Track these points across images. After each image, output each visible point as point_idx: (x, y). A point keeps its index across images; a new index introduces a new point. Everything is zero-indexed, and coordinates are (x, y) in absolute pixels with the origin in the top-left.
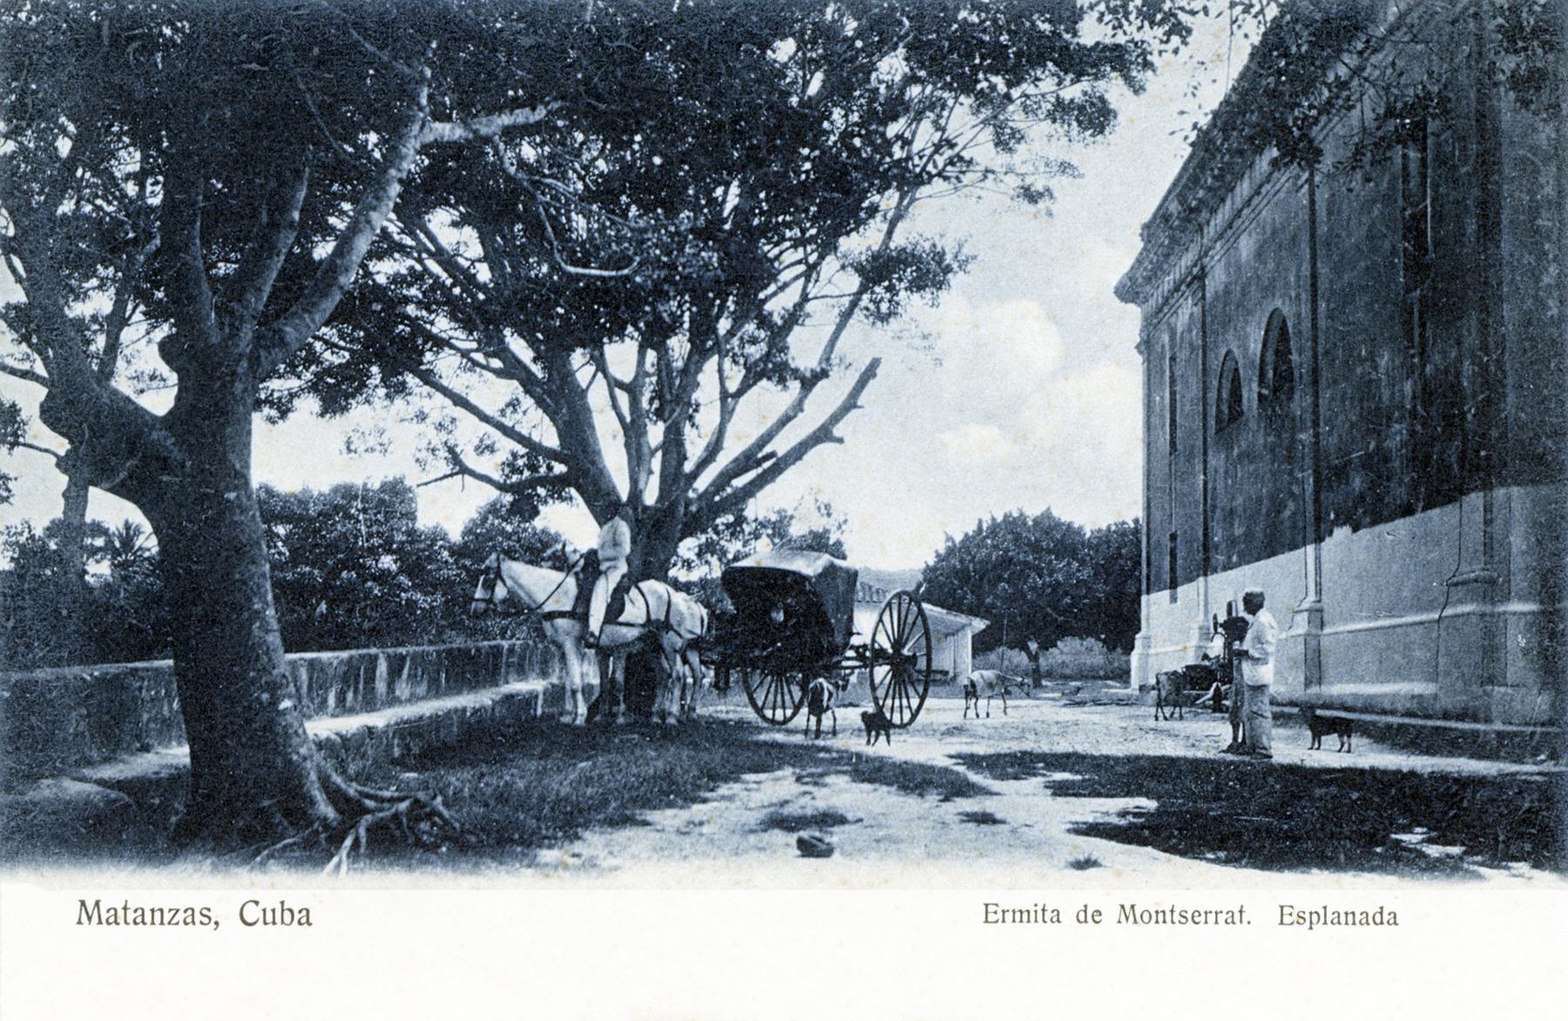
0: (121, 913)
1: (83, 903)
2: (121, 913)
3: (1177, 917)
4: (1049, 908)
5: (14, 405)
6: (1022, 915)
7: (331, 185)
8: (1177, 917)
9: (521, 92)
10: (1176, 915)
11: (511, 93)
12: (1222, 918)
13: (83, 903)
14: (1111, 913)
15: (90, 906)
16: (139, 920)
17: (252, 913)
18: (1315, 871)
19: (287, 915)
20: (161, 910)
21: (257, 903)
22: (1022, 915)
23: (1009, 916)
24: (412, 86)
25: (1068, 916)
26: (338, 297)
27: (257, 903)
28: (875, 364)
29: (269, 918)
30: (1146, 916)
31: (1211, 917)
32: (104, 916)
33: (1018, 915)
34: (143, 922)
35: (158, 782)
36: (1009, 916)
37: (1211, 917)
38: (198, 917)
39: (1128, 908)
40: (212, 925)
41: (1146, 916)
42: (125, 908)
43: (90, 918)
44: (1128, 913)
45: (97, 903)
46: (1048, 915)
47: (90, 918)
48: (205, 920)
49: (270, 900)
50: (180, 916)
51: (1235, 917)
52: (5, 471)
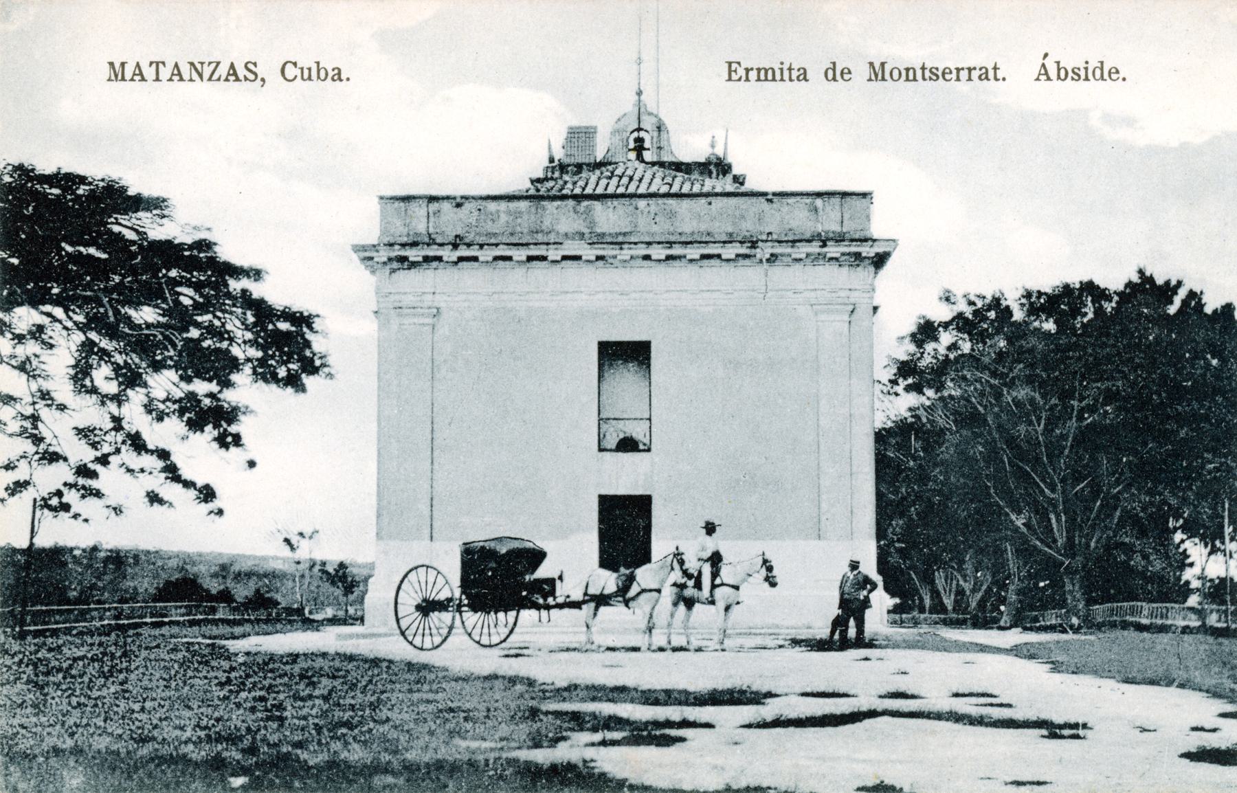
3: (927, 74)
5: (137, 432)
7: (24, 232)
12: (975, 74)
14: (861, 72)
18: (1223, 748)
20: (924, 79)
21: (295, 64)
23: (753, 75)
25: (815, 74)
27: (295, 64)
28: (1195, 729)
30: (896, 73)
31: (964, 74)
36: (753, 75)
37: (964, 74)
40: (258, 81)
41: (896, 73)
45: (883, 64)
46: (795, 74)
48: (252, 77)
52: (6, 390)
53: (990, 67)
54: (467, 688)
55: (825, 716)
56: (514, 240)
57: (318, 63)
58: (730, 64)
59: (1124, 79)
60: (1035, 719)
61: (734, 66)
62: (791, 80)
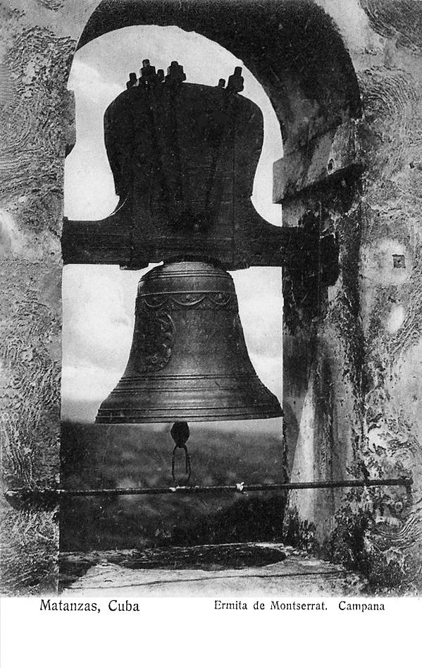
0: (58, 605)
1: (43, 601)
2: (58, 605)
3: (296, 607)
4: (242, 603)
6: (229, 606)
8: (296, 607)
9: (145, 530)
10: (296, 606)
11: (141, 527)
13: (43, 601)
14: (268, 605)
15: (46, 602)
16: (136, 609)
17: (114, 606)
19: (129, 606)
21: (116, 601)
22: (229, 606)
24: (217, 482)
25: (250, 606)
26: (234, 487)
27: (116, 601)
29: (121, 608)
31: (310, 607)
32: (51, 607)
33: (229, 606)
34: (72, 604)
35: (217, 562)
36: (225, 606)
38: (91, 607)
39: (275, 603)
41: (283, 607)
42: (60, 603)
43: (45, 608)
44: (275, 605)
46: (242, 606)
47: (45, 608)
48: (94, 609)
49: (122, 601)
50: (83, 607)
51: (321, 607)
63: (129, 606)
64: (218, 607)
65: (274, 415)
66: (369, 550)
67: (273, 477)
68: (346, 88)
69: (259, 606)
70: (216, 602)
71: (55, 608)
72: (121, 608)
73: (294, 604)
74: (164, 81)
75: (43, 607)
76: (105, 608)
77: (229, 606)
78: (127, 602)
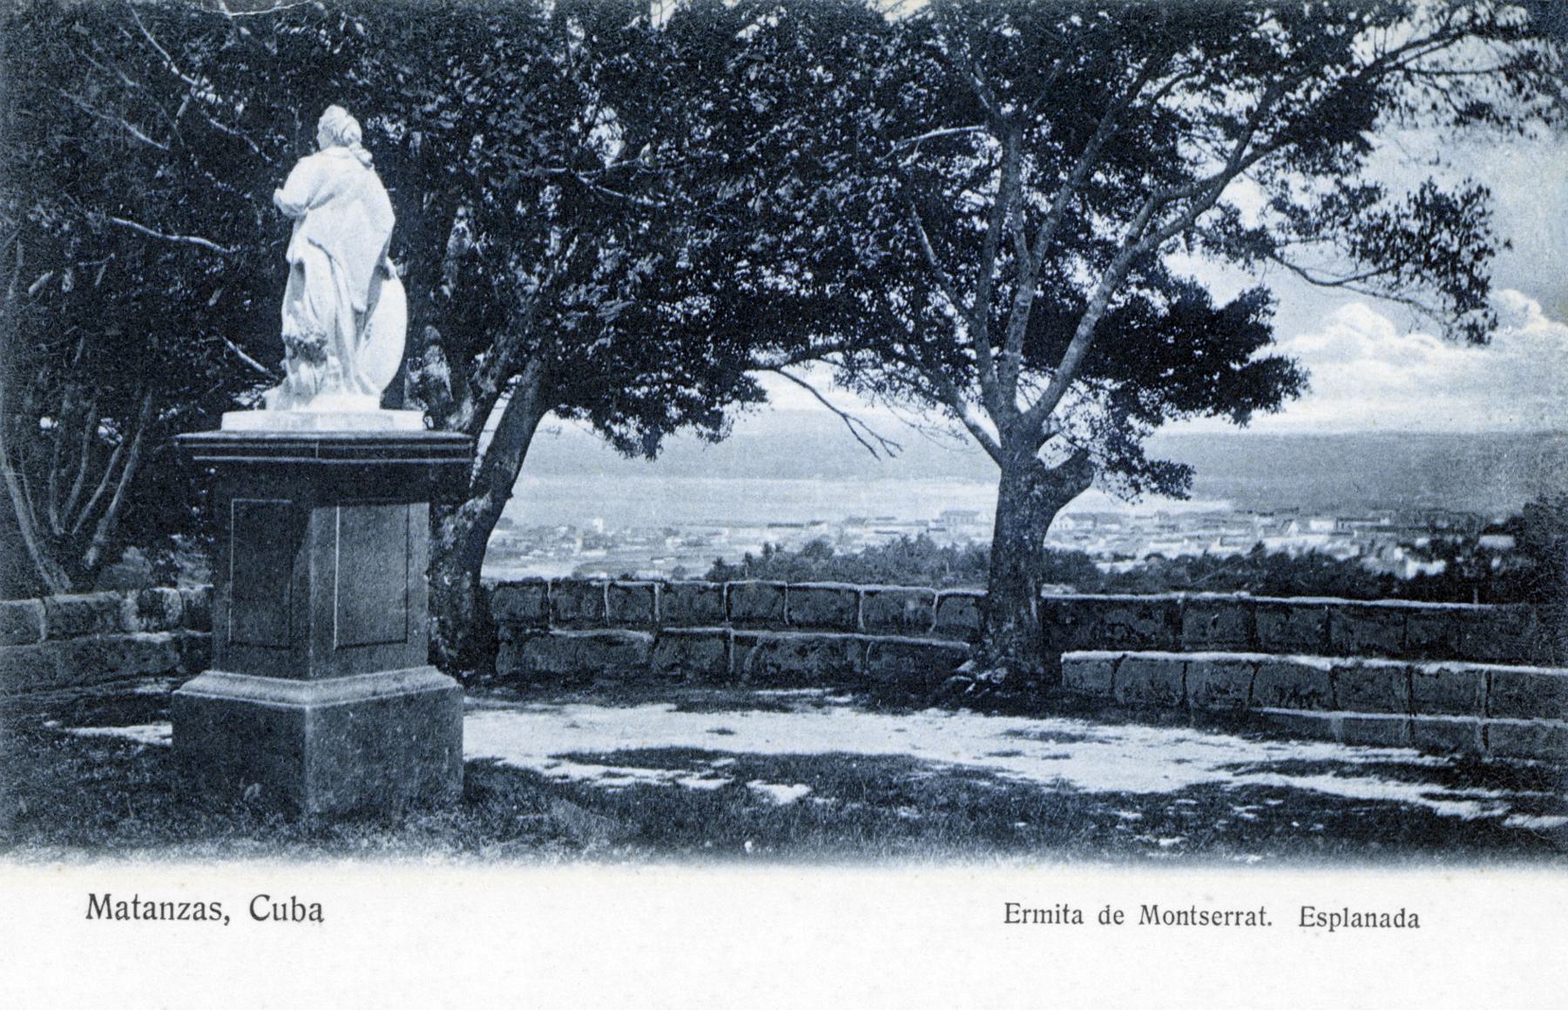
3: (1197, 918)
12: (1243, 919)
14: (1133, 915)
16: (315, 916)
17: (262, 908)
19: (299, 911)
20: (171, 905)
21: (267, 897)
23: (1030, 916)
25: (1090, 917)
27: (267, 897)
29: (280, 914)
31: (1232, 919)
33: (1039, 915)
36: (1030, 916)
38: (208, 912)
40: (223, 920)
43: (99, 913)
44: (1150, 914)
47: (99, 913)
48: (215, 915)
50: (191, 911)
51: (1256, 918)
53: (1189, 910)
54: (361, 650)
55: (641, 752)
56: (317, 308)
57: (294, 899)
58: (1008, 905)
59: (1508, 244)
60: (587, 751)
61: (1013, 908)
62: (136, 917)
63: (299, 911)
64: (1013, 917)
65: (527, 421)
66: (753, 352)
67: (606, 517)
68: (401, 77)
69: (1110, 917)
70: (1008, 905)
71: (121, 914)
72: (280, 914)
73: (135, 903)
74: (1236, 367)
75: (94, 913)
76: (240, 915)
77: (1039, 915)
78: (294, 899)
